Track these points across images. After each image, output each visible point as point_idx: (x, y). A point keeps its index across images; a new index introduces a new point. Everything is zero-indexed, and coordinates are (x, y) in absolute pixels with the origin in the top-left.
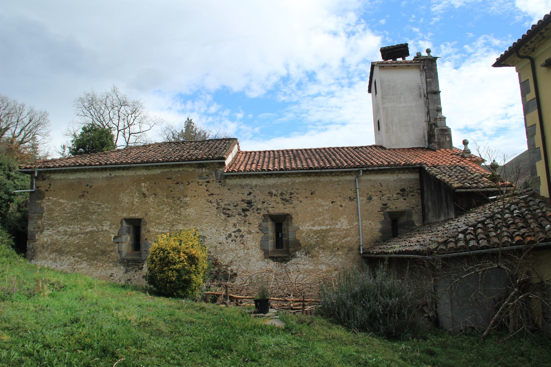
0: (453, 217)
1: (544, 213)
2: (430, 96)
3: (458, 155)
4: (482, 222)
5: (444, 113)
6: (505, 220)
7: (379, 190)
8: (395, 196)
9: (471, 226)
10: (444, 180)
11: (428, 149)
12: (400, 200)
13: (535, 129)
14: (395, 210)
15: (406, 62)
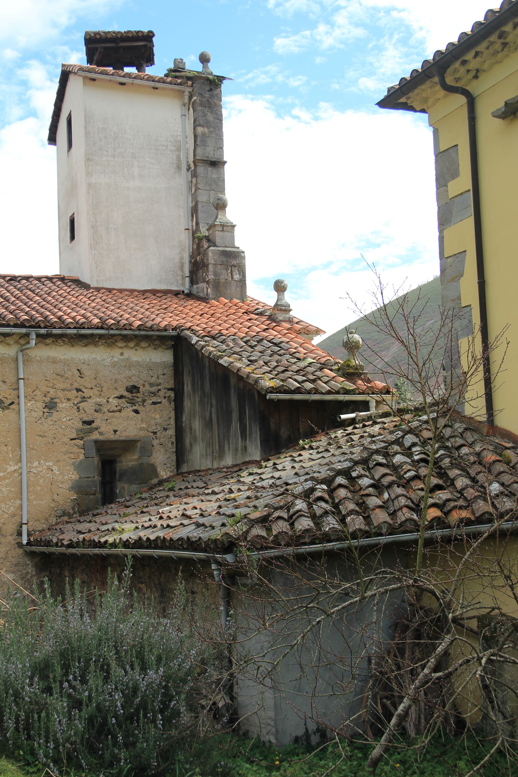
0: (257, 457)
1: (478, 454)
2: (201, 170)
3: (261, 314)
4: (346, 473)
5: (231, 214)
6: (395, 468)
7: (76, 385)
8: (114, 402)
9: (322, 482)
10: (239, 369)
11: (190, 296)
12: (124, 413)
13: (463, 262)
14: (112, 437)
15: (151, 79)
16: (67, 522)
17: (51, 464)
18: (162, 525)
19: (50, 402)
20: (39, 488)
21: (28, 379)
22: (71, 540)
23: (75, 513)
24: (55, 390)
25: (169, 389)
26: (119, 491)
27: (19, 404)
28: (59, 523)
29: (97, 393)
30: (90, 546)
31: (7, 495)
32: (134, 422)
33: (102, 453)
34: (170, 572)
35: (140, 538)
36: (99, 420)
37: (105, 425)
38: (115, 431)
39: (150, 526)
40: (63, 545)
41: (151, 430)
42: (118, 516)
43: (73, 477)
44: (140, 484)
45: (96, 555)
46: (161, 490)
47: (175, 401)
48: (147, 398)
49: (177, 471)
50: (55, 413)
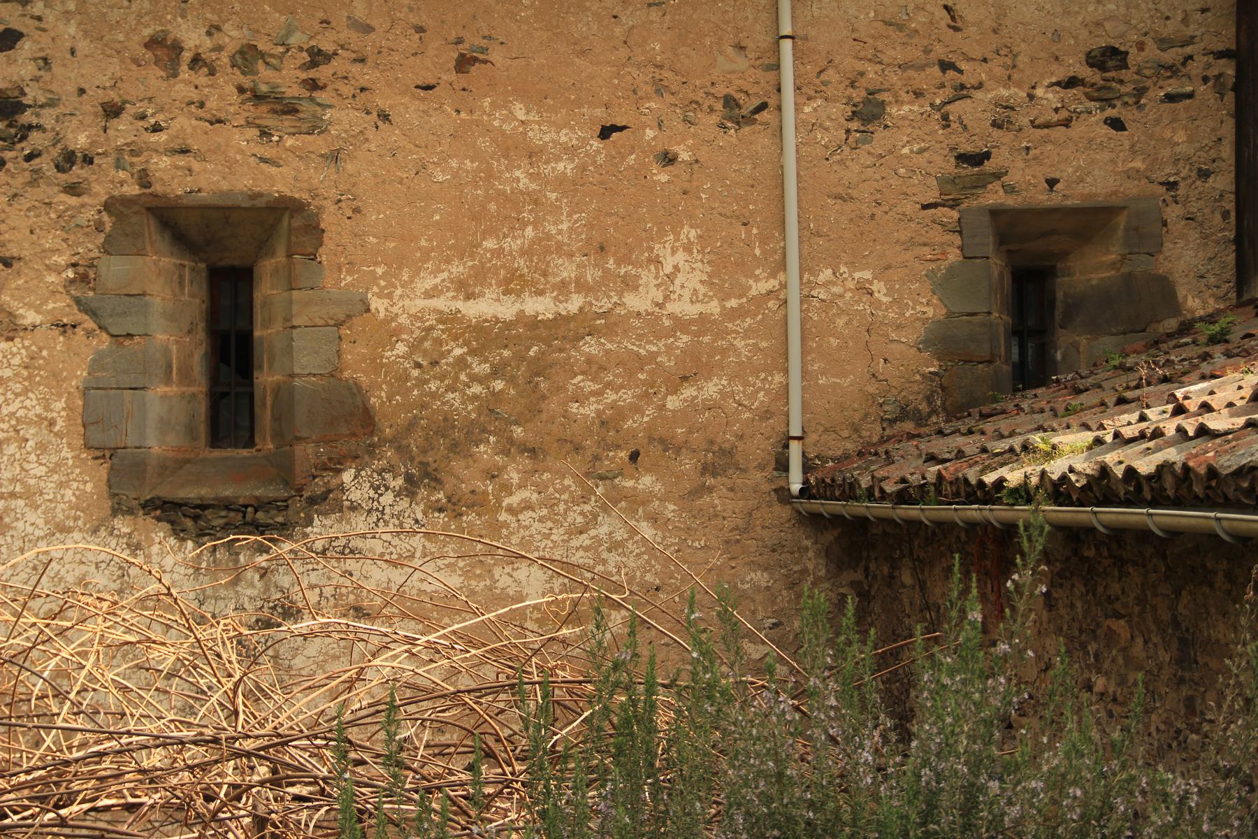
7: (939, 51)
8: (1049, 97)
12: (1078, 129)
14: (1043, 198)
16: (911, 437)
17: (867, 275)
18: (1180, 430)
19: (867, 102)
20: (834, 342)
21: (806, 38)
22: (903, 480)
23: (934, 412)
24: (878, 67)
25: (1220, 55)
26: (1064, 358)
27: (779, 108)
28: (890, 438)
29: (999, 71)
30: (955, 498)
31: (749, 359)
32: (1106, 156)
33: (1013, 247)
34: (1211, 585)
35: (1104, 471)
36: (1004, 151)
37: (1021, 164)
38: (1052, 183)
39: (1142, 436)
40: (884, 496)
41: (1159, 176)
42: (1048, 414)
43: (930, 312)
44: (1125, 333)
45: (972, 525)
46: (1186, 344)
47: (1236, 88)
48: (1149, 83)
49: (1239, 295)
50: (880, 134)
